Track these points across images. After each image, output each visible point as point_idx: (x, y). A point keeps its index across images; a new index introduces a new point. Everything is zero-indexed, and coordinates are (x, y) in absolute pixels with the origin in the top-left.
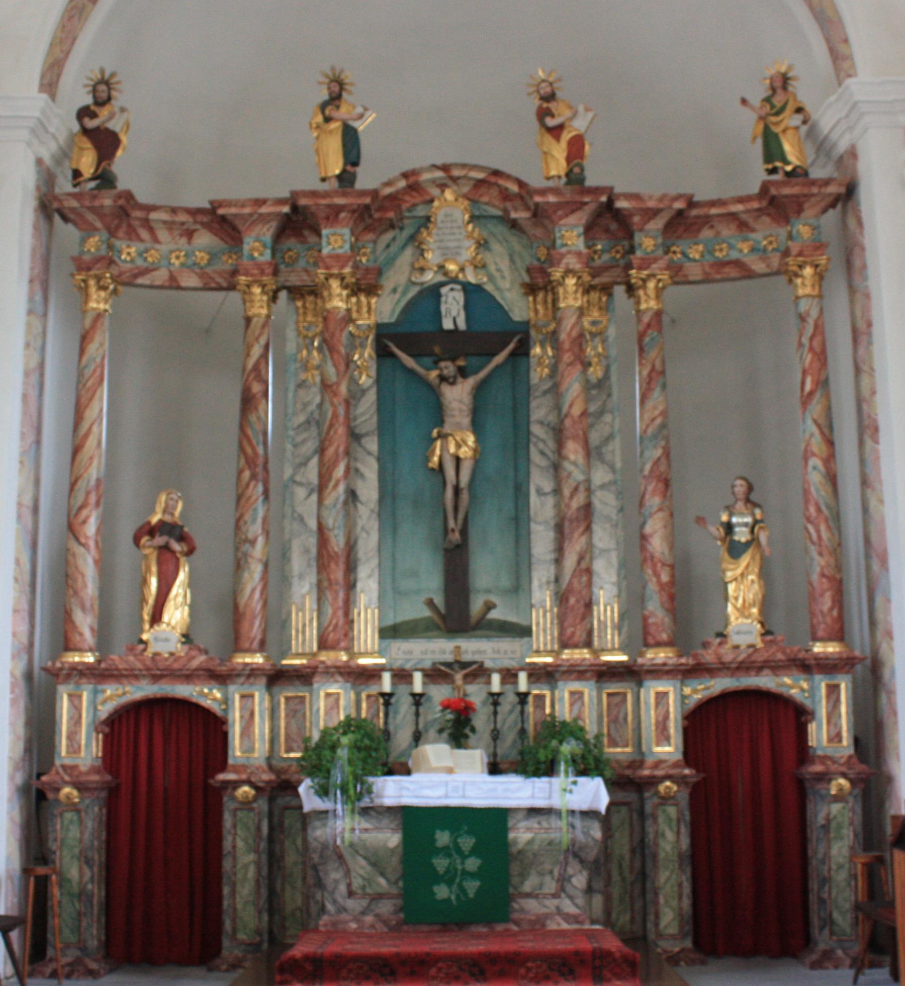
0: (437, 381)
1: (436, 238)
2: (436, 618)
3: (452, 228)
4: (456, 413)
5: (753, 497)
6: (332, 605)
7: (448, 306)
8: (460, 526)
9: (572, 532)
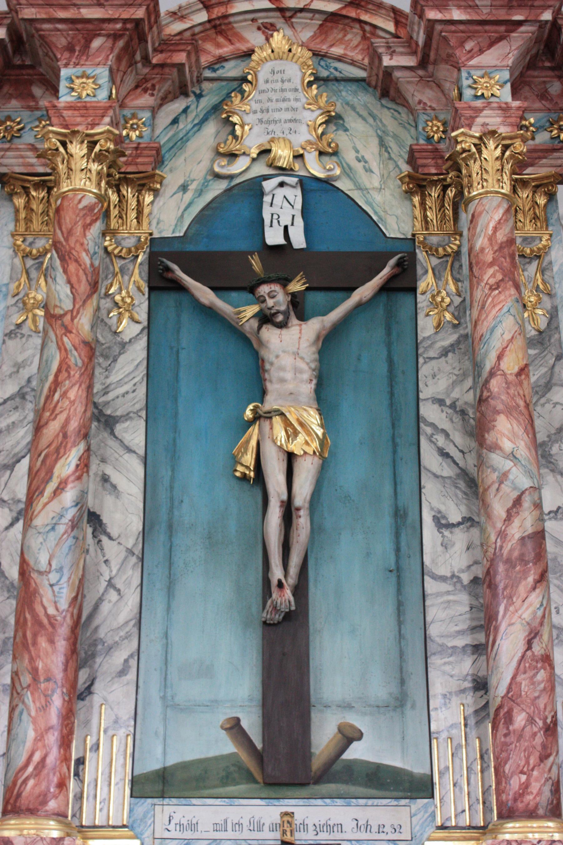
0: (255, 324)
1: (256, 106)
2: (245, 757)
3: (282, 90)
4: (289, 376)
5: (356, 822)
6: (35, 721)
7: (274, 210)
8: (292, 579)
9: (513, 585)
